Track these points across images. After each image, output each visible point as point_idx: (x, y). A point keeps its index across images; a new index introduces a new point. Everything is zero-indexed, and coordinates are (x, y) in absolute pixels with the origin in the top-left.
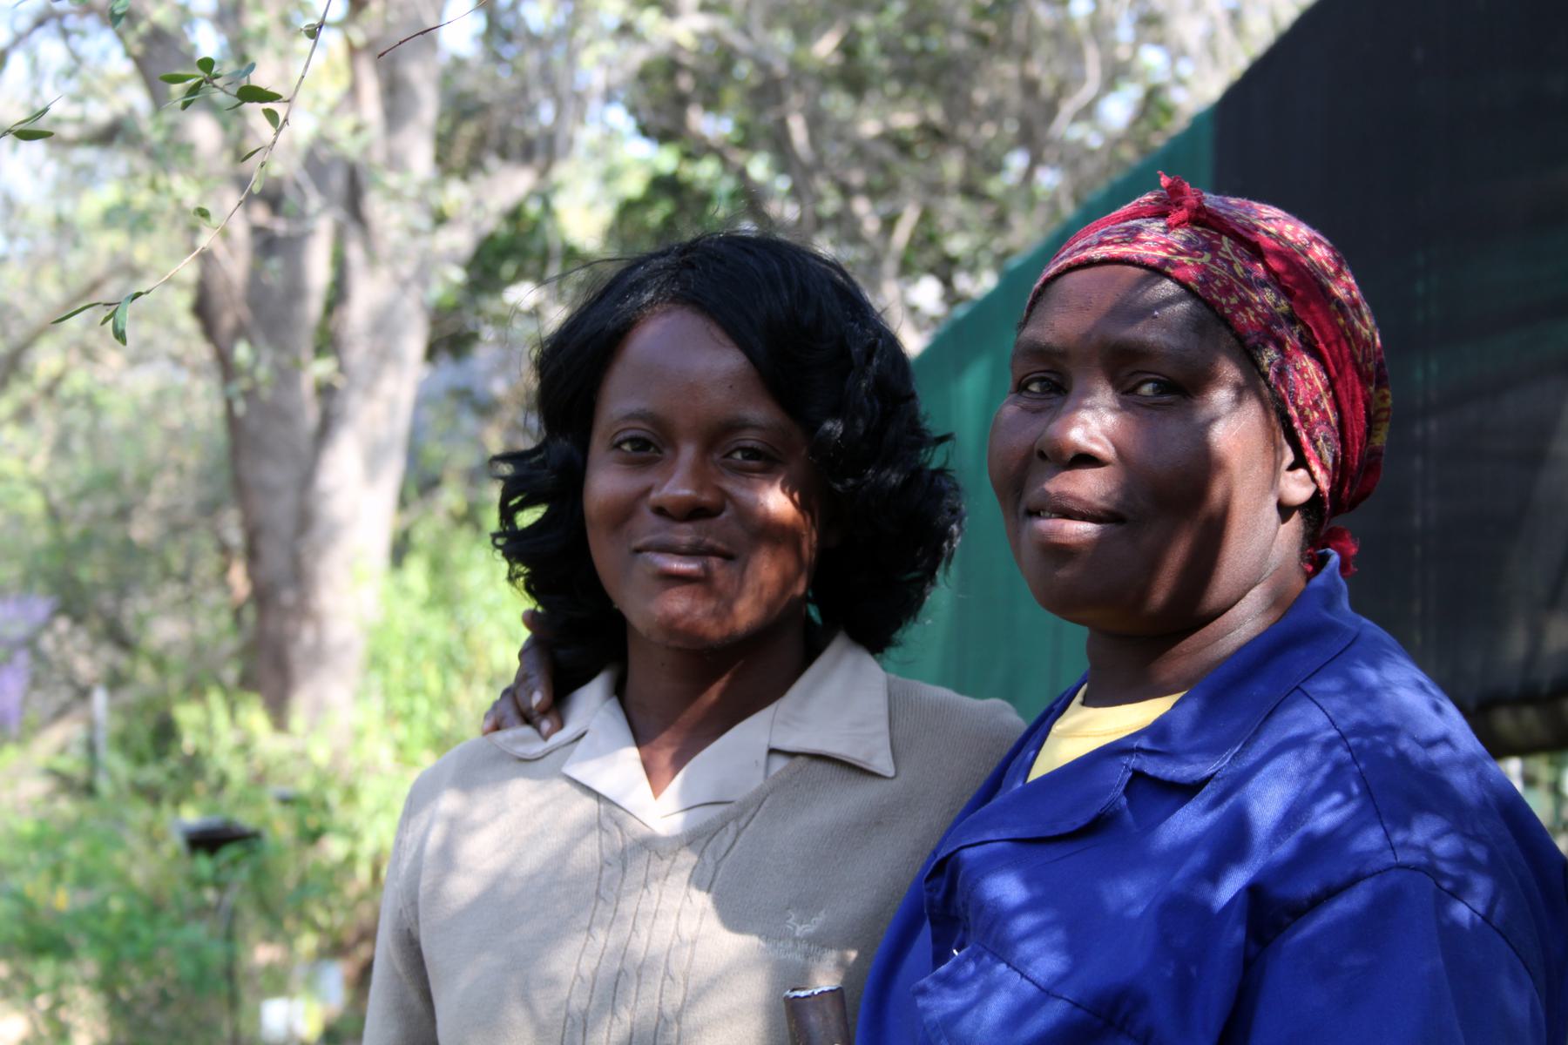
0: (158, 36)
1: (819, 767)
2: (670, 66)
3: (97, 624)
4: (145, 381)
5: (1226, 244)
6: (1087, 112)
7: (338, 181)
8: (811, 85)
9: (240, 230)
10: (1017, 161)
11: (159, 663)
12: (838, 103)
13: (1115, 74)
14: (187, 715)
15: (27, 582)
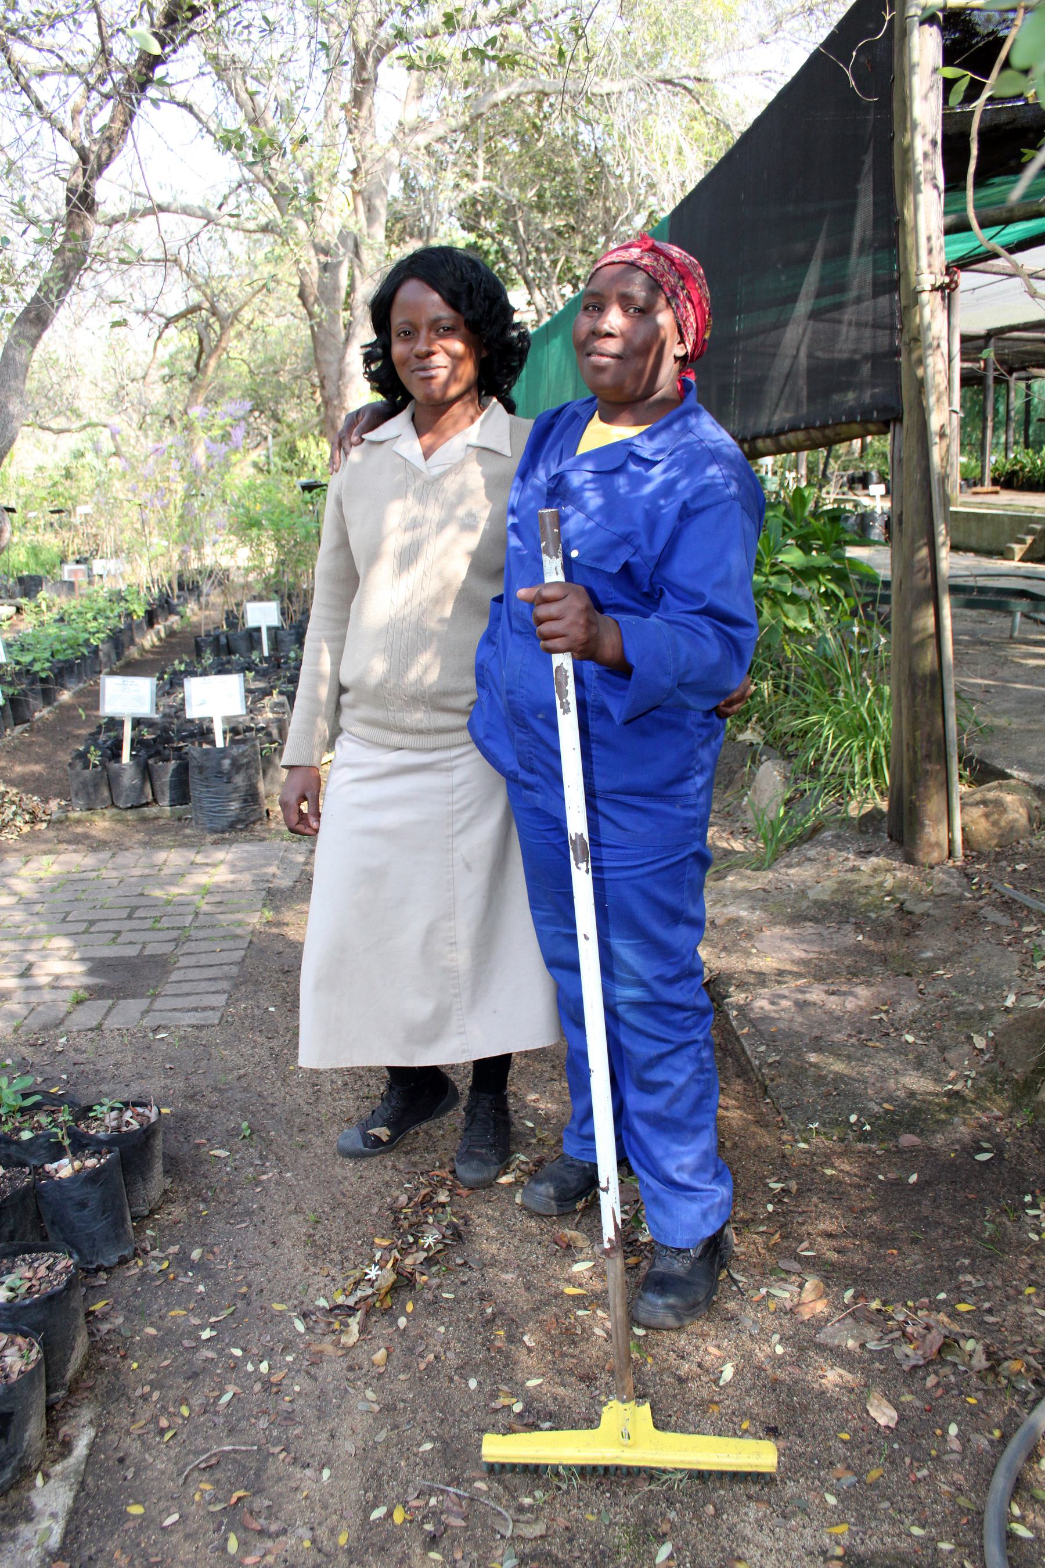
0: (282, 187)
1: (485, 452)
2: (474, 202)
3: (268, 413)
4: (282, 323)
5: (662, 259)
6: (628, 220)
7: (350, 243)
8: (525, 209)
9: (315, 264)
10: (602, 240)
11: (289, 426)
12: (536, 216)
13: (639, 206)
14: (301, 444)
15: (243, 396)
